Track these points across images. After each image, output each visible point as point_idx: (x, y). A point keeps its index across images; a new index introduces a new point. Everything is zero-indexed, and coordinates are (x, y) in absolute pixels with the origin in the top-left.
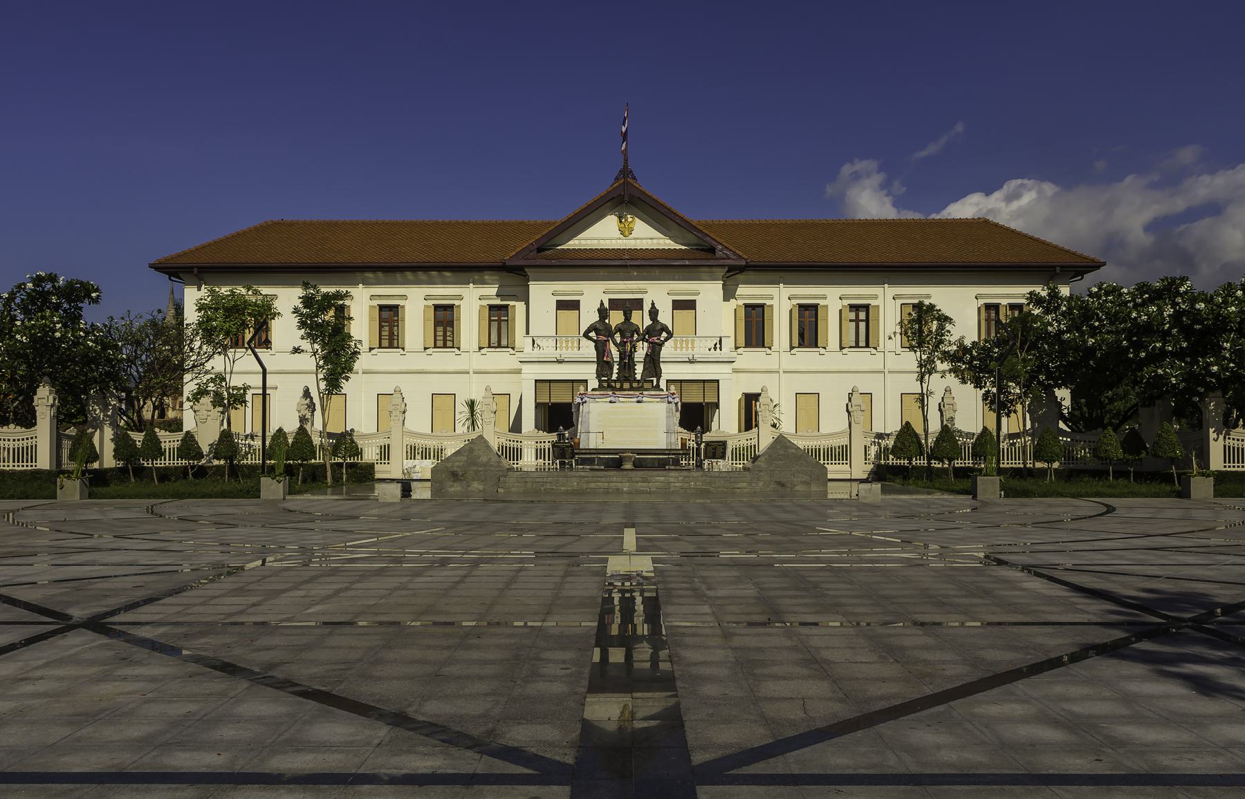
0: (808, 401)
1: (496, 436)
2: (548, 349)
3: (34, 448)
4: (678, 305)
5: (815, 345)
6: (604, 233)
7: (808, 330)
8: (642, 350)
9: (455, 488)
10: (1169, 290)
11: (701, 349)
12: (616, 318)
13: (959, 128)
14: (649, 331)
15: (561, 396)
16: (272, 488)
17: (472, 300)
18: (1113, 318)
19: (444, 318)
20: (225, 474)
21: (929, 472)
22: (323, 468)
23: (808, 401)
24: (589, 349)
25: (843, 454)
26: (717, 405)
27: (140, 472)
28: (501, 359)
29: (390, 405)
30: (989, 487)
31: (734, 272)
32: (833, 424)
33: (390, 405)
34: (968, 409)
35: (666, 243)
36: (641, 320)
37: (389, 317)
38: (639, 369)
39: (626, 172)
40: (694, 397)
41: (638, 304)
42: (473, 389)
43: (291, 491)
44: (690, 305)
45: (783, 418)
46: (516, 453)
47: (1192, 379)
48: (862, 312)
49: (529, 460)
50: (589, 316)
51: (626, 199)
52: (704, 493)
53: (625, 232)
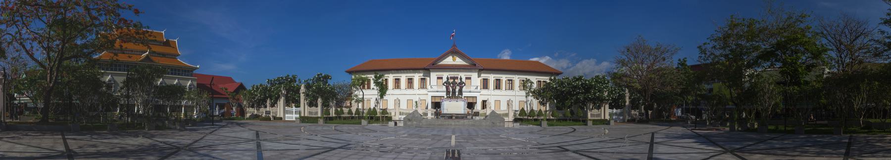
0: (498, 102)
1: (421, 112)
2: (435, 88)
3: (871, 118)
4: (467, 78)
6: (449, 60)
7: (498, 86)
9: (409, 123)
10: (580, 78)
11: (473, 89)
12: (451, 81)
15: (438, 100)
16: (364, 122)
17: (417, 77)
18: (569, 84)
19: (410, 81)
20: (356, 118)
21: (528, 120)
22: (379, 117)
23: (498, 102)
24: (444, 88)
25: (507, 115)
27: (340, 117)
28: (424, 91)
29: (398, 102)
30: (545, 123)
31: (481, 71)
32: (504, 108)
33: (398, 102)
34: (535, 105)
35: (464, 63)
36: (458, 81)
37: (397, 81)
39: (454, 45)
40: (471, 101)
42: (416, 98)
43: (369, 123)
44: (470, 78)
45: (491, 107)
46: (426, 114)
47: (585, 99)
48: (511, 81)
49: (430, 116)
50: (445, 80)
51: (454, 52)
52: (474, 125)
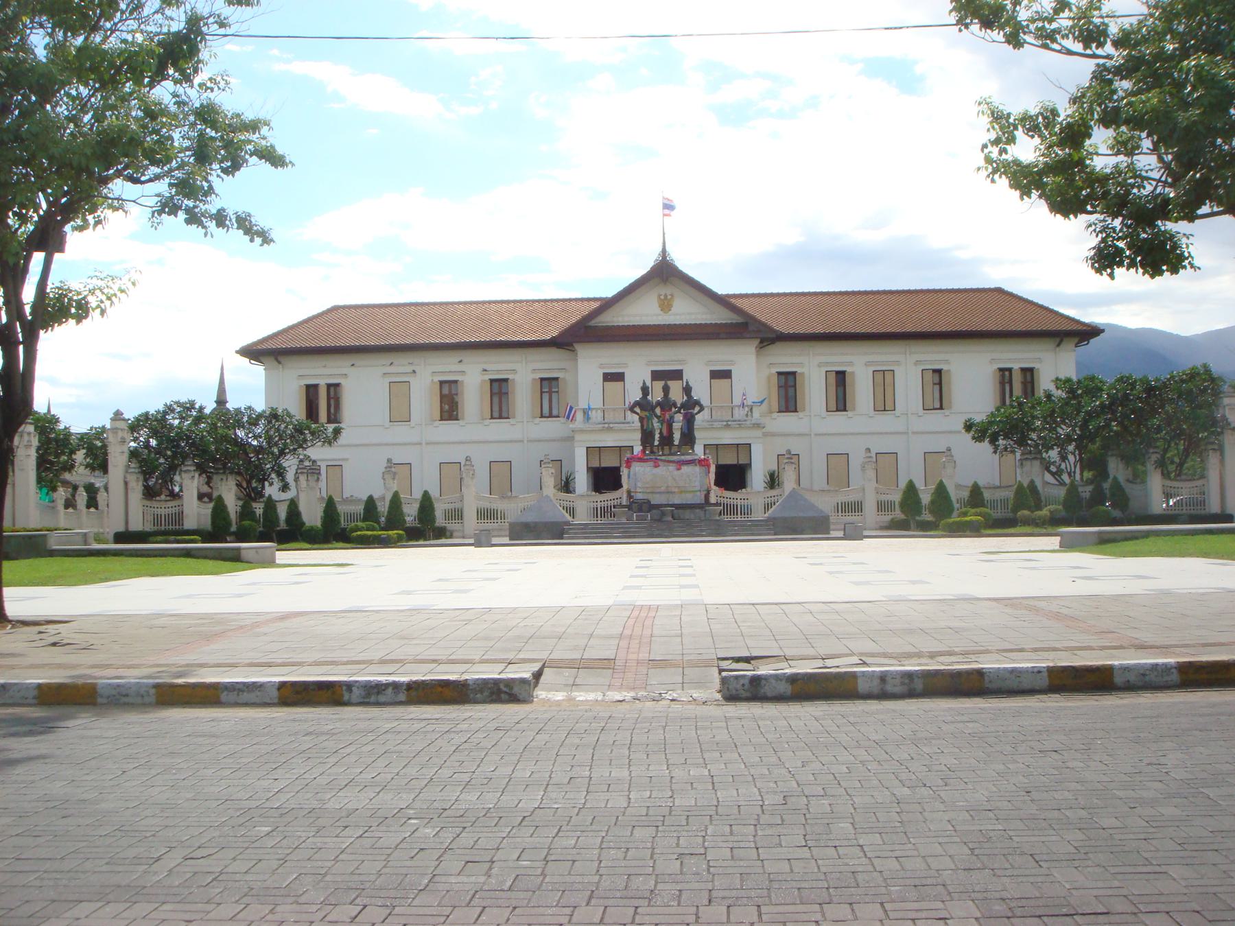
14: (683, 406)
19: (499, 390)
40: (729, 459)
41: (677, 375)
53: (666, 305)
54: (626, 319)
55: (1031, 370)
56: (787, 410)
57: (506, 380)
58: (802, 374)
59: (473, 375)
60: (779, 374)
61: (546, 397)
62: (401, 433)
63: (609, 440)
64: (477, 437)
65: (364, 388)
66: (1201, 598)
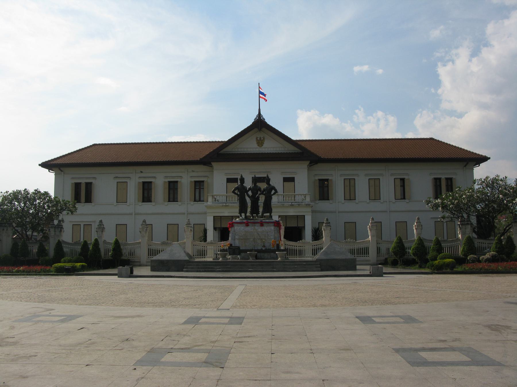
5: (150, 201)
8: (262, 199)
13: (380, 71)
26: (304, 227)
28: (198, 207)
38: (261, 210)
40: (293, 224)
53: (260, 143)
54: (240, 150)
55: (451, 179)
56: (324, 199)
57: (177, 182)
58: (331, 180)
59: (160, 178)
60: (320, 180)
61: (197, 191)
62: (123, 208)
63: (226, 213)
64: (161, 212)
65: (105, 185)
66: (110, 270)
